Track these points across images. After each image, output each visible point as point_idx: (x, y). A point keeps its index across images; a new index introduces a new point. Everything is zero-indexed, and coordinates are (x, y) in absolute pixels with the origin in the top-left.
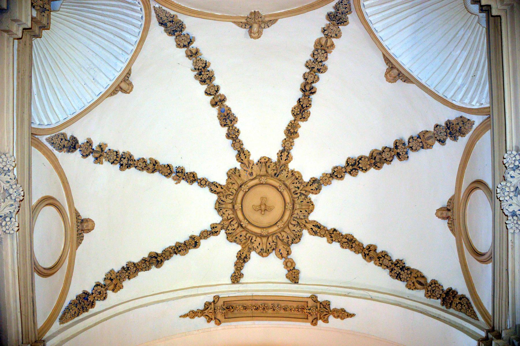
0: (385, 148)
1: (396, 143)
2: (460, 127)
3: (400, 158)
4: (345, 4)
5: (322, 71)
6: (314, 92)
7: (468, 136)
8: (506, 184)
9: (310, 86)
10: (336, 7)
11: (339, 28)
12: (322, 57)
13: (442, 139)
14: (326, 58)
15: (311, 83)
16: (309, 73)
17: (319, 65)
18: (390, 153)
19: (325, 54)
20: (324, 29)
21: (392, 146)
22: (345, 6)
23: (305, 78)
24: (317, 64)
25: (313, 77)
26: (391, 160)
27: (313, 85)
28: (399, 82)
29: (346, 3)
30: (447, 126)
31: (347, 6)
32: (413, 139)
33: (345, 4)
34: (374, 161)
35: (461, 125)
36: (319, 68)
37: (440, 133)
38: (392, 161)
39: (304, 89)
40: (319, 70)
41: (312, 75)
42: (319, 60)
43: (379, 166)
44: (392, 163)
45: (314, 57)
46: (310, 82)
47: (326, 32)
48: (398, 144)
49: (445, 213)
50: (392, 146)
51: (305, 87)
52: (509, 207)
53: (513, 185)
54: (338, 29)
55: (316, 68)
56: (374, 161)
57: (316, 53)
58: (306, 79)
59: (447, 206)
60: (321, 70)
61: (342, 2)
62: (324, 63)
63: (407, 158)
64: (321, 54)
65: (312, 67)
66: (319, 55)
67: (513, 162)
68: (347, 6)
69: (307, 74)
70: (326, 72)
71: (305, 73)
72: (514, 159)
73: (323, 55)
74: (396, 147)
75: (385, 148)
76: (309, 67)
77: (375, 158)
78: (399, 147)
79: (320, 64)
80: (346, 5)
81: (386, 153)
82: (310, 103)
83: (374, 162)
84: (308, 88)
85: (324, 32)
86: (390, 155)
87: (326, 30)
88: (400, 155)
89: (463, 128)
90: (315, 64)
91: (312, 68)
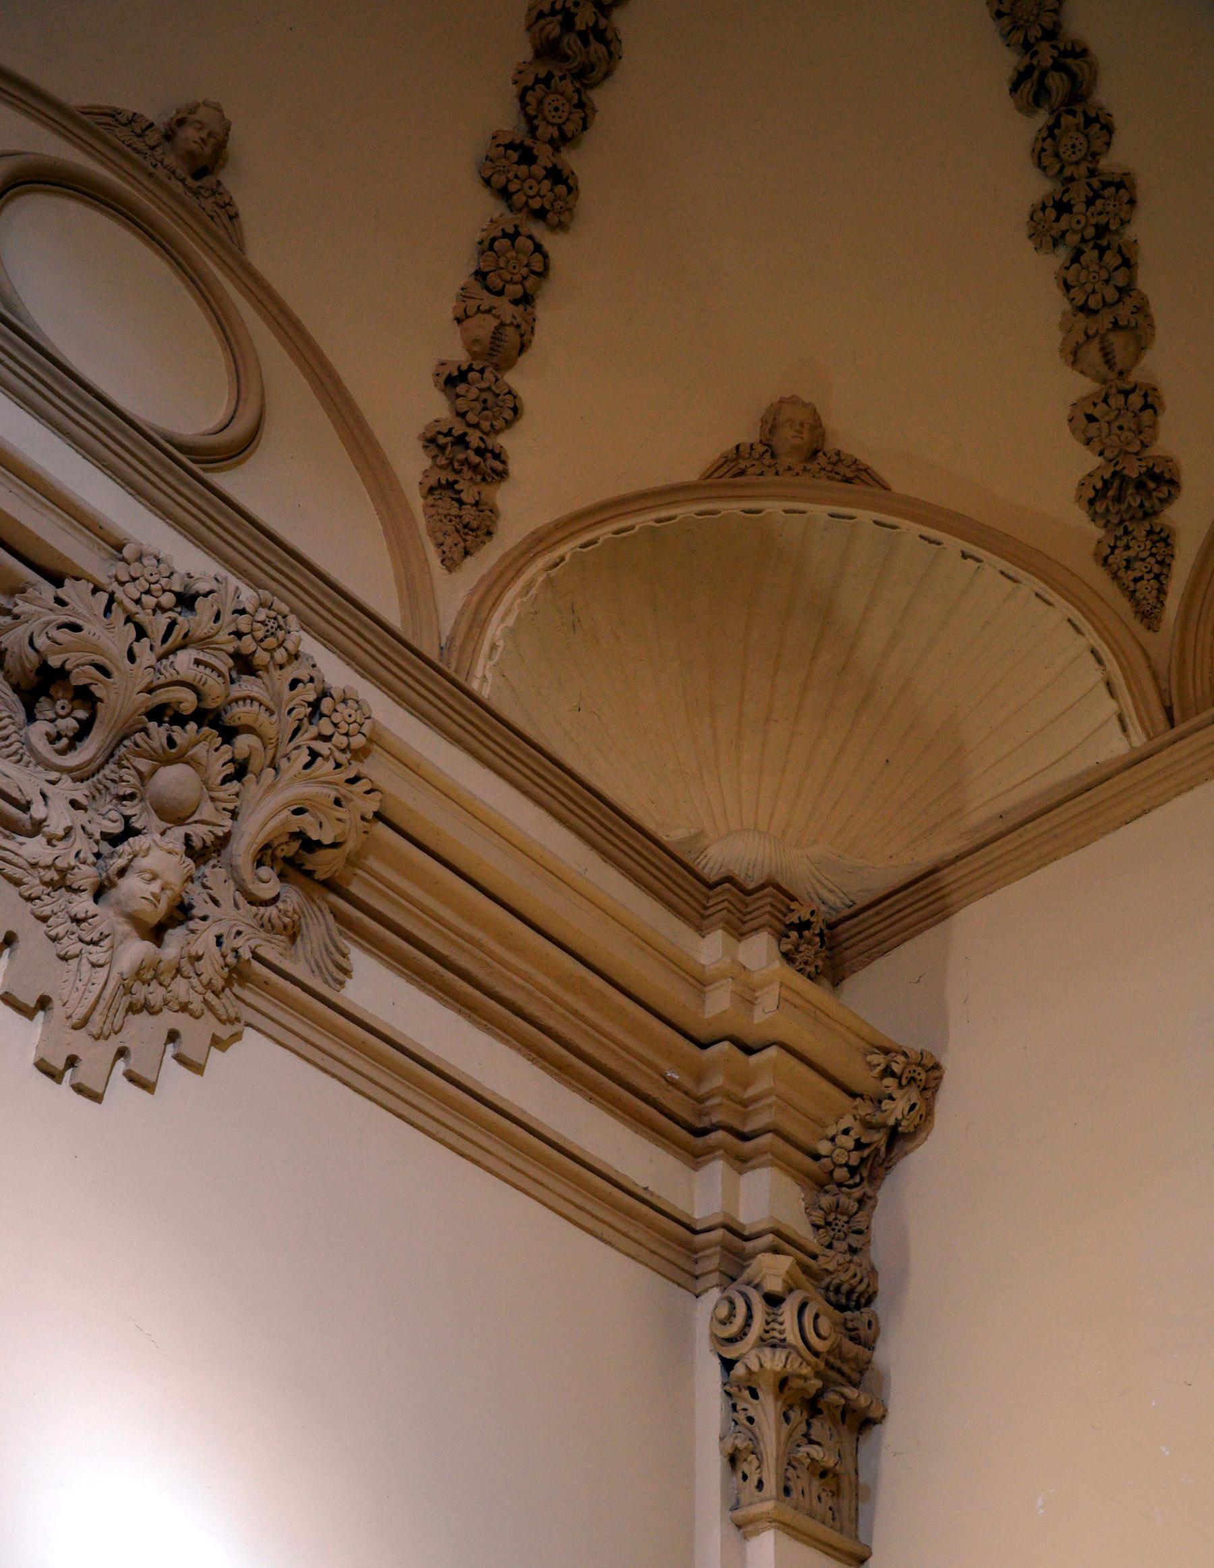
0: (584, 120)
1: (570, 190)
2: (461, 503)
3: (510, 152)
4: (1142, 578)
5: (1048, 211)
6: (1015, 87)
7: (417, 502)
8: (272, 658)
9: (1056, 98)
10: (1163, 539)
11: (1101, 454)
12: (1083, 280)
13: (461, 388)
14: (1067, 287)
15: (1057, 124)
16: (1095, 156)
17: (1074, 232)
18: (553, 125)
19: (1080, 299)
20: (1152, 407)
21: (571, 159)
22: (1138, 574)
23: (1097, 119)
24: (1085, 228)
25: (1065, 157)
26: (528, 99)
27: (1043, 118)
28: (745, 432)
29: (1139, 585)
30: (492, 451)
31: (1132, 575)
32: (533, 272)
33: (1142, 578)
34: (580, 25)
35: (469, 514)
36: (1065, 217)
37: (485, 401)
38: (522, 98)
39: (1070, 61)
40: (1062, 207)
41: (1074, 158)
42: (1090, 255)
43: (542, 22)
44: (514, 90)
45: (1120, 251)
46: (1067, 120)
47: (1136, 400)
48: (561, 189)
49: (189, 136)
50: (571, 159)
51: (1072, 76)
52: (215, 608)
53: (271, 668)
54: (1099, 447)
55: (1079, 207)
56: (580, 25)
57: (1120, 278)
58: (1089, 121)
59: (219, 183)
60: (1051, 213)
61: (1157, 577)
62: (1063, 254)
63: (487, 174)
64: (1098, 286)
65: (1099, 202)
66: (1104, 275)
67: (336, 718)
68: (1132, 575)
69: (1097, 145)
70: (1027, 219)
71: (1108, 144)
72: (344, 728)
73: (1089, 288)
74: (557, 175)
75: (584, 120)
76: (1112, 190)
77: (586, 43)
78: (547, 184)
79: (1073, 239)
80: (1136, 580)
81: (567, 108)
82: (1006, 20)
83: (577, 20)
84: (1057, 82)
85: (1145, 396)
86: (549, 117)
87: (1142, 409)
88: (519, 163)
89: (455, 511)
90: (1093, 221)
91: (1097, 195)
